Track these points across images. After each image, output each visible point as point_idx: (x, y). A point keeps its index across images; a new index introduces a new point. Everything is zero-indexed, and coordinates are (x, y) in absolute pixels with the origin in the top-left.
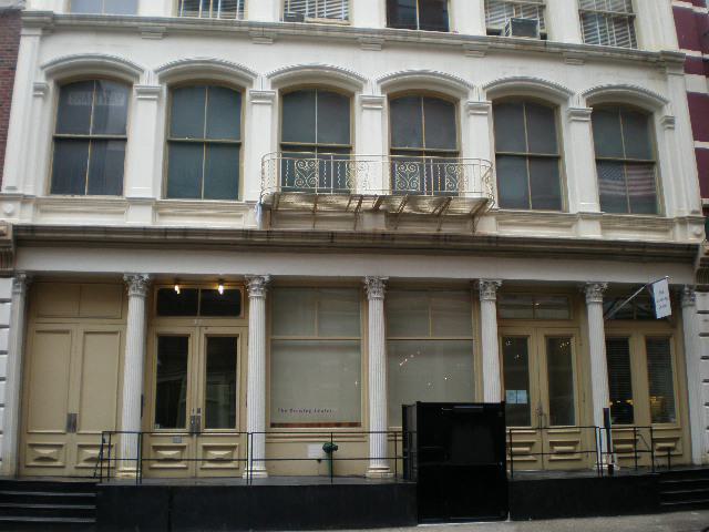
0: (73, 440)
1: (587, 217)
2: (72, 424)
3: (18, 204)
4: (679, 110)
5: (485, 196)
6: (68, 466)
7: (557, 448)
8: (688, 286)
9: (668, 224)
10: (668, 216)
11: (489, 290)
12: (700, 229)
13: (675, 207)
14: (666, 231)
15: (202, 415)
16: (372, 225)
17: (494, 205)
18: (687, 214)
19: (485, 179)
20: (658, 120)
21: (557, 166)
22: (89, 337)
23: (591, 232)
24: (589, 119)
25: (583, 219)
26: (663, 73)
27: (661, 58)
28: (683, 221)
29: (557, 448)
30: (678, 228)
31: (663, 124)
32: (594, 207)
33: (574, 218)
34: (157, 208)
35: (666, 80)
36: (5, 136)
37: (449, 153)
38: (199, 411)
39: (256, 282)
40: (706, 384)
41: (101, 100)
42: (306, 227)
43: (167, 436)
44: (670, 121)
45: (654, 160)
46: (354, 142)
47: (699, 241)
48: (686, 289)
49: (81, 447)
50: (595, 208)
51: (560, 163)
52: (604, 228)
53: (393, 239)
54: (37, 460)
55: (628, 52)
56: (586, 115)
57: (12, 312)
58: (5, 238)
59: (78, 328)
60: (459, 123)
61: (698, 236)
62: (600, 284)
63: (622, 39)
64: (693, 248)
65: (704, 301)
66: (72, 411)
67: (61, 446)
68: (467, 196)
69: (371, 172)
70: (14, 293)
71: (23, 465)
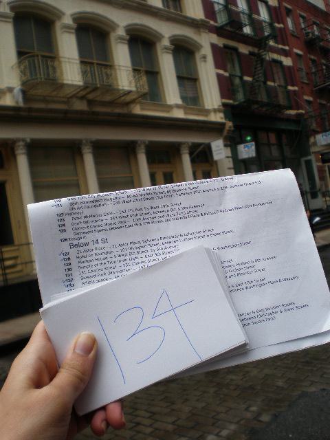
1: (178, 106)
4: (207, 51)
9: (207, 112)
10: (207, 107)
11: (143, 146)
12: (222, 115)
14: (168, 112)
16: (80, 106)
20: (198, 56)
23: (179, 114)
24: (11, 20)
26: (199, 31)
27: (200, 23)
28: (215, 111)
31: (201, 58)
35: (200, 35)
37: (51, 55)
42: (42, 106)
44: (204, 57)
47: (224, 121)
50: (180, 102)
51: (56, 63)
52: (186, 113)
55: (177, 14)
56: (72, 29)
60: (111, 48)
61: (222, 118)
62: (188, 143)
63: (176, 8)
64: (223, 125)
69: (72, 73)
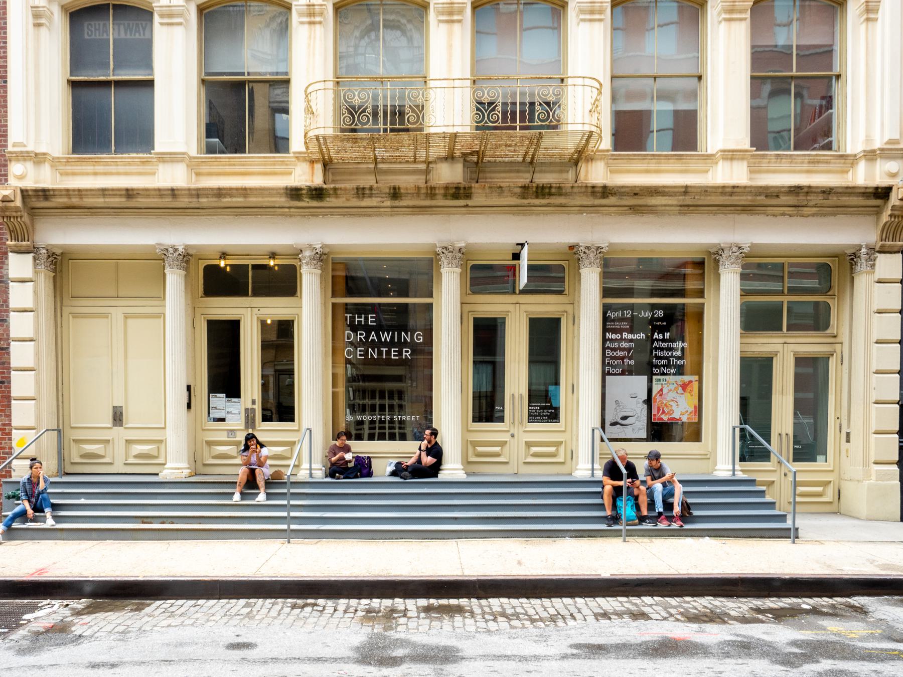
0: (119, 434)
2: (118, 417)
3: (29, 165)
5: (587, 128)
6: (116, 463)
7: (534, 449)
8: (867, 247)
9: (850, 161)
13: (862, 137)
15: (258, 407)
17: (606, 143)
18: (877, 144)
19: (595, 108)
21: (288, 88)
22: (130, 321)
24: (748, 15)
25: (725, 159)
29: (534, 449)
30: (862, 165)
32: (742, 139)
33: (850, 161)
34: (193, 165)
36: (4, 79)
38: (254, 402)
39: (307, 253)
40: (876, 375)
41: (122, 32)
43: (488, 431)
45: (836, 70)
46: (844, 63)
48: (864, 250)
49: (128, 442)
53: (198, 196)
54: (82, 456)
57: (35, 292)
58: (12, 204)
59: (117, 314)
65: (888, 265)
66: (117, 404)
67: (108, 441)
68: (570, 128)
70: (36, 273)
71: (199, 463)
